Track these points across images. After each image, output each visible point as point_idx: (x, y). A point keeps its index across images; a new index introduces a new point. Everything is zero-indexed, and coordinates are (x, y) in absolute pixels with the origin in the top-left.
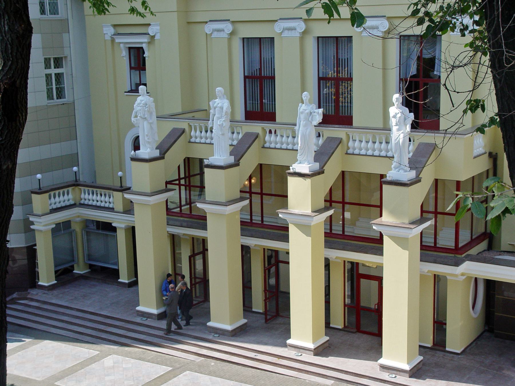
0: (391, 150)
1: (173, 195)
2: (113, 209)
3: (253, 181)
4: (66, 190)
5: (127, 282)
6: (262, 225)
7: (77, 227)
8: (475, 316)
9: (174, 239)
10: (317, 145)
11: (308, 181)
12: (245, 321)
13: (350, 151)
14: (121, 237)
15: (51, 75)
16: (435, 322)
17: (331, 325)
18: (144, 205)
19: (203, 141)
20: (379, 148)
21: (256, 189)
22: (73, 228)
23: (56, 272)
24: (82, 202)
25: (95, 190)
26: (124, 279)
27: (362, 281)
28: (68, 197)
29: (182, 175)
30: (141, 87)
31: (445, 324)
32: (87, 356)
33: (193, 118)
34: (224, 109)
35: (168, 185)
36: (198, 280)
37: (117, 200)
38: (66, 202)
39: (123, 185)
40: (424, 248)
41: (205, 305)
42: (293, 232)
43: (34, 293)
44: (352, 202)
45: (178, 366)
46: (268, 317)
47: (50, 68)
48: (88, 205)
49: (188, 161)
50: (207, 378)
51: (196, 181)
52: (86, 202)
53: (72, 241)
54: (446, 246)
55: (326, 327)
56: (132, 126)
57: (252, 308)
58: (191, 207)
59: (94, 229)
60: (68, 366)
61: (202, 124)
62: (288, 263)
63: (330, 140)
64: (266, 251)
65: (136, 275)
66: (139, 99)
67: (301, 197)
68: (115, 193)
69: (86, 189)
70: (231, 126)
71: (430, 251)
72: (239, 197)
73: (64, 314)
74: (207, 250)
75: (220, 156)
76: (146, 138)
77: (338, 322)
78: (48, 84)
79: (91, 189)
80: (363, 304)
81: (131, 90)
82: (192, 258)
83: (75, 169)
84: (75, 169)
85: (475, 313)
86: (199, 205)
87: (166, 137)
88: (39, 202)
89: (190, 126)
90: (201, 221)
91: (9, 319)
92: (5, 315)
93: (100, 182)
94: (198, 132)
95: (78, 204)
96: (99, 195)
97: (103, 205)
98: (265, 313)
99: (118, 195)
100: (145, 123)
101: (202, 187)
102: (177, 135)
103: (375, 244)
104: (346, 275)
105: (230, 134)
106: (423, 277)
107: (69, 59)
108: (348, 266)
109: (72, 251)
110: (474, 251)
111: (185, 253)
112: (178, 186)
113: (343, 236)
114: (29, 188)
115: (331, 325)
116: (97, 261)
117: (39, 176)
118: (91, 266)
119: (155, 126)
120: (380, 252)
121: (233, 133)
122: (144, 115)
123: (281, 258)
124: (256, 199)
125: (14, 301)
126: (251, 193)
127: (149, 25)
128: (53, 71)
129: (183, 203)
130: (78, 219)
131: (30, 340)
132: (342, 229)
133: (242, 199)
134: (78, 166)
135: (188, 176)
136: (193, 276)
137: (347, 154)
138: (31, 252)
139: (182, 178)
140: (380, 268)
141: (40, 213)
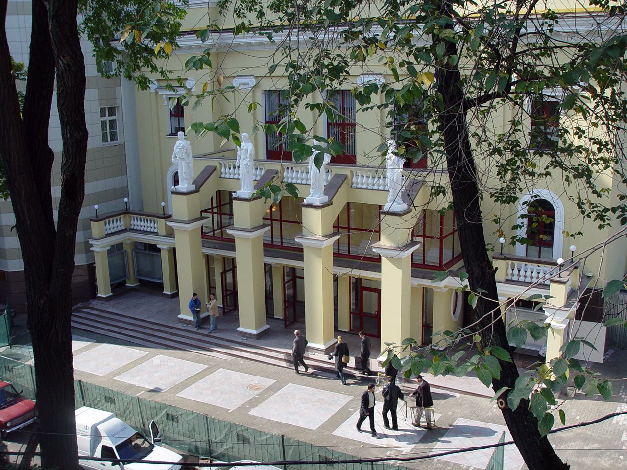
0: (310, 179)
1: (207, 222)
2: (157, 233)
3: (273, 209)
4: (118, 218)
5: (170, 293)
6: (281, 247)
7: (128, 248)
8: (455, 320)
9: (208, 258)
10: (327, 181)
11: (319, 211)
12: (268, 326)
13: (354, 185)
14: (165, 257)
15: (105, 122)
16: (423, 326)
17: (339, 329)
18: (182, 230)
19: (231, 176)
20: (379, 183)
21: (276, 216)
22: (124, 249)
23: (112, 286)
24: (132, 227)
25: (142, 217)
26: (167, 291)
27: (365, 292)
28: (119, 224)
29: (214, 205)
30: (180, 133)
31: (432, 327)
32: (139, 356)
33: (223, 158)
34: (249, 151)
35: (203, 213)
36: (228, 292)
37: (160, 226)
38: (119, 227)
39: (166, 213)
40: (414, 266)
41: (235, 312)
42: (385, 263)
43: (94, 303)
44: (355, 227)
45: (214, 364)
46: (287, 323)
47: (105, 116)
48: (137, 230)
49: (219, 193)
50: (237, 373)
51: (226, 209)
52: (135, 227)
53: (124, 259)
54: (433, 263)
55: (334, 330)
56: (172, 164)
57: (273, 315)
58: (222, 231)
59: (141, 250)
60: (123, 365)
61: (231, 162)
62: (303, 278)
63: (337, 176)
64: (285, 268)
65: (178, 289)
66: (178, 142)
67: (316, 224)
68: (158, 219)
69: (135, 216)
70: (255, 165)
71: (419, 268)
72: (262, 224)
73: (131, 324)
74: (236, 267)
75: (245, 190)
76: (184, 175)
77: (345, 326)
78: (103, 130)
79: (139, 217)
80: (365, 310)
81: (172, 133)
82: (224, 275)
83: (126, 200)
84: (126, 200)
85: (455, 318)
86: (229, 231)
87: (201, 173)
88: (96, 228)
89: (352, 173)
90: (230, 243)
91: (72, 324)
92: (69, 320)
93: (147, 210)
94: (227, 169)
95: (128, 229)
96: (146, 221)
97: (149, 229)
98: (285, 319)
99: (161, 221)
100: (183, 163)
101: (231, 215)
102: (210, 171)
103: (374, 262)
104: (352, 286)
105: (254, 171)
106: (414, 289)
107: (120, 108)
108: (353, 280)
109: (124, 266)
110: (454, 268)
111: (218, 270)
112: (211, 214)
113: (349, 256)
114: (89, 216)
115: (339, 329)
116: (145, 276)
117: (96, 206)
118: (140, 280)
119: (191, 165)
120: (378, 269)
121: (257, 169)
122: (182, 156)
123: (298, 274)
124: (276, 225)
125: (78, 310)
126: (272, 220)
127: (187, 79)
128: (107, 118)
129: (216, 227)
130: (129, 242)
131: (89, 343)
132: (422, 259)
133: (264, 226)
134: (128, 197)
135: (220, 206)
136: (225, 289)
137: (351, 188)
138: (91, 269)
139: (215, 207)
140: (379, 282)
141: (98, 237)
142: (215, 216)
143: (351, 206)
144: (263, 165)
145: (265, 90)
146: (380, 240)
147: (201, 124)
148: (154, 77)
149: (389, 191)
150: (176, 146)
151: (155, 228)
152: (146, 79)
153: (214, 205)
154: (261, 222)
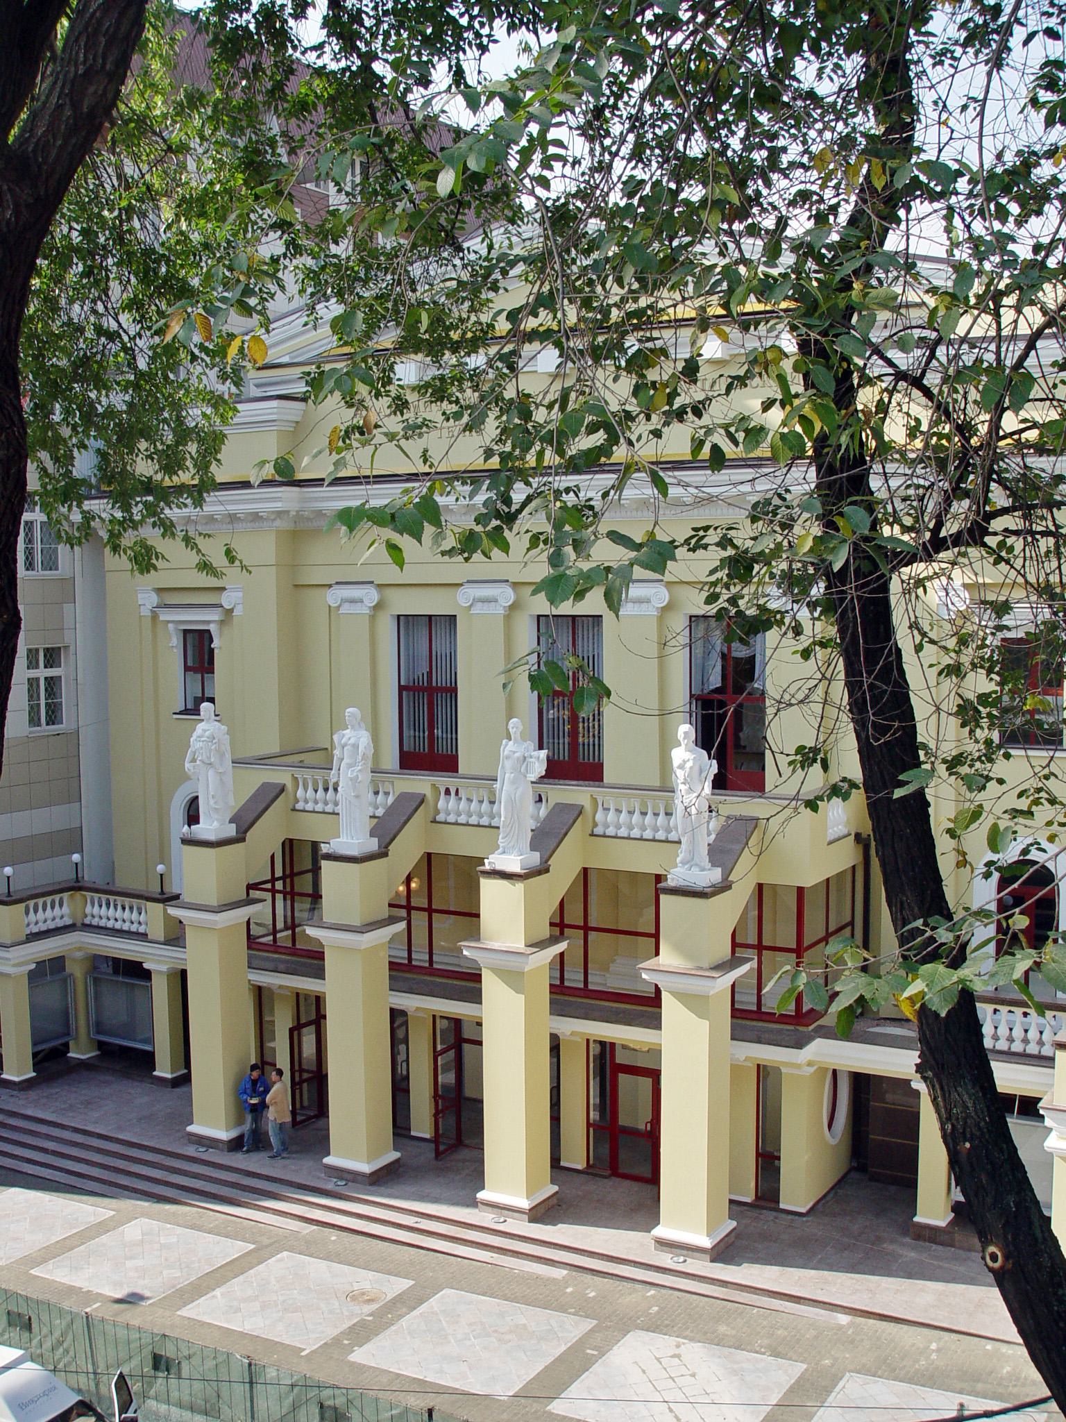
1: (261, 911)
3: (413, 885)
10: (536, 818)
11: (520, 886)
19: (319, 807)
20: (652, 825)
29: (279, 873)
30: (205, 706)
33: (301, 765)
39: (166, 889)
49: (289, 846)
56: (185, 777)
61: (319, 775)
63: (561, 808)
66: (201, 726)
70: (373, 781)
75: (352, 837)
76: (212, 802)
89: (594, 801)
100: (211, 773)
101: (316, 896)
102: (270, 795)
105: (371, 795)
121: (376, 793)
122: (209, 758)
124: (420, 919)
126: (409, 908)
129: (280, 925)
133: (392, 920)
135: (290, 875)
137: (592, 835)
139: (279, 879)
142: (279, 897)
143: (592, 878)
145: (399, 616)
146: (657, 954)
149: (679, 842)
150: (195, 735)
151: (140, 923)
153: (279, 873)
154: (385, 912)
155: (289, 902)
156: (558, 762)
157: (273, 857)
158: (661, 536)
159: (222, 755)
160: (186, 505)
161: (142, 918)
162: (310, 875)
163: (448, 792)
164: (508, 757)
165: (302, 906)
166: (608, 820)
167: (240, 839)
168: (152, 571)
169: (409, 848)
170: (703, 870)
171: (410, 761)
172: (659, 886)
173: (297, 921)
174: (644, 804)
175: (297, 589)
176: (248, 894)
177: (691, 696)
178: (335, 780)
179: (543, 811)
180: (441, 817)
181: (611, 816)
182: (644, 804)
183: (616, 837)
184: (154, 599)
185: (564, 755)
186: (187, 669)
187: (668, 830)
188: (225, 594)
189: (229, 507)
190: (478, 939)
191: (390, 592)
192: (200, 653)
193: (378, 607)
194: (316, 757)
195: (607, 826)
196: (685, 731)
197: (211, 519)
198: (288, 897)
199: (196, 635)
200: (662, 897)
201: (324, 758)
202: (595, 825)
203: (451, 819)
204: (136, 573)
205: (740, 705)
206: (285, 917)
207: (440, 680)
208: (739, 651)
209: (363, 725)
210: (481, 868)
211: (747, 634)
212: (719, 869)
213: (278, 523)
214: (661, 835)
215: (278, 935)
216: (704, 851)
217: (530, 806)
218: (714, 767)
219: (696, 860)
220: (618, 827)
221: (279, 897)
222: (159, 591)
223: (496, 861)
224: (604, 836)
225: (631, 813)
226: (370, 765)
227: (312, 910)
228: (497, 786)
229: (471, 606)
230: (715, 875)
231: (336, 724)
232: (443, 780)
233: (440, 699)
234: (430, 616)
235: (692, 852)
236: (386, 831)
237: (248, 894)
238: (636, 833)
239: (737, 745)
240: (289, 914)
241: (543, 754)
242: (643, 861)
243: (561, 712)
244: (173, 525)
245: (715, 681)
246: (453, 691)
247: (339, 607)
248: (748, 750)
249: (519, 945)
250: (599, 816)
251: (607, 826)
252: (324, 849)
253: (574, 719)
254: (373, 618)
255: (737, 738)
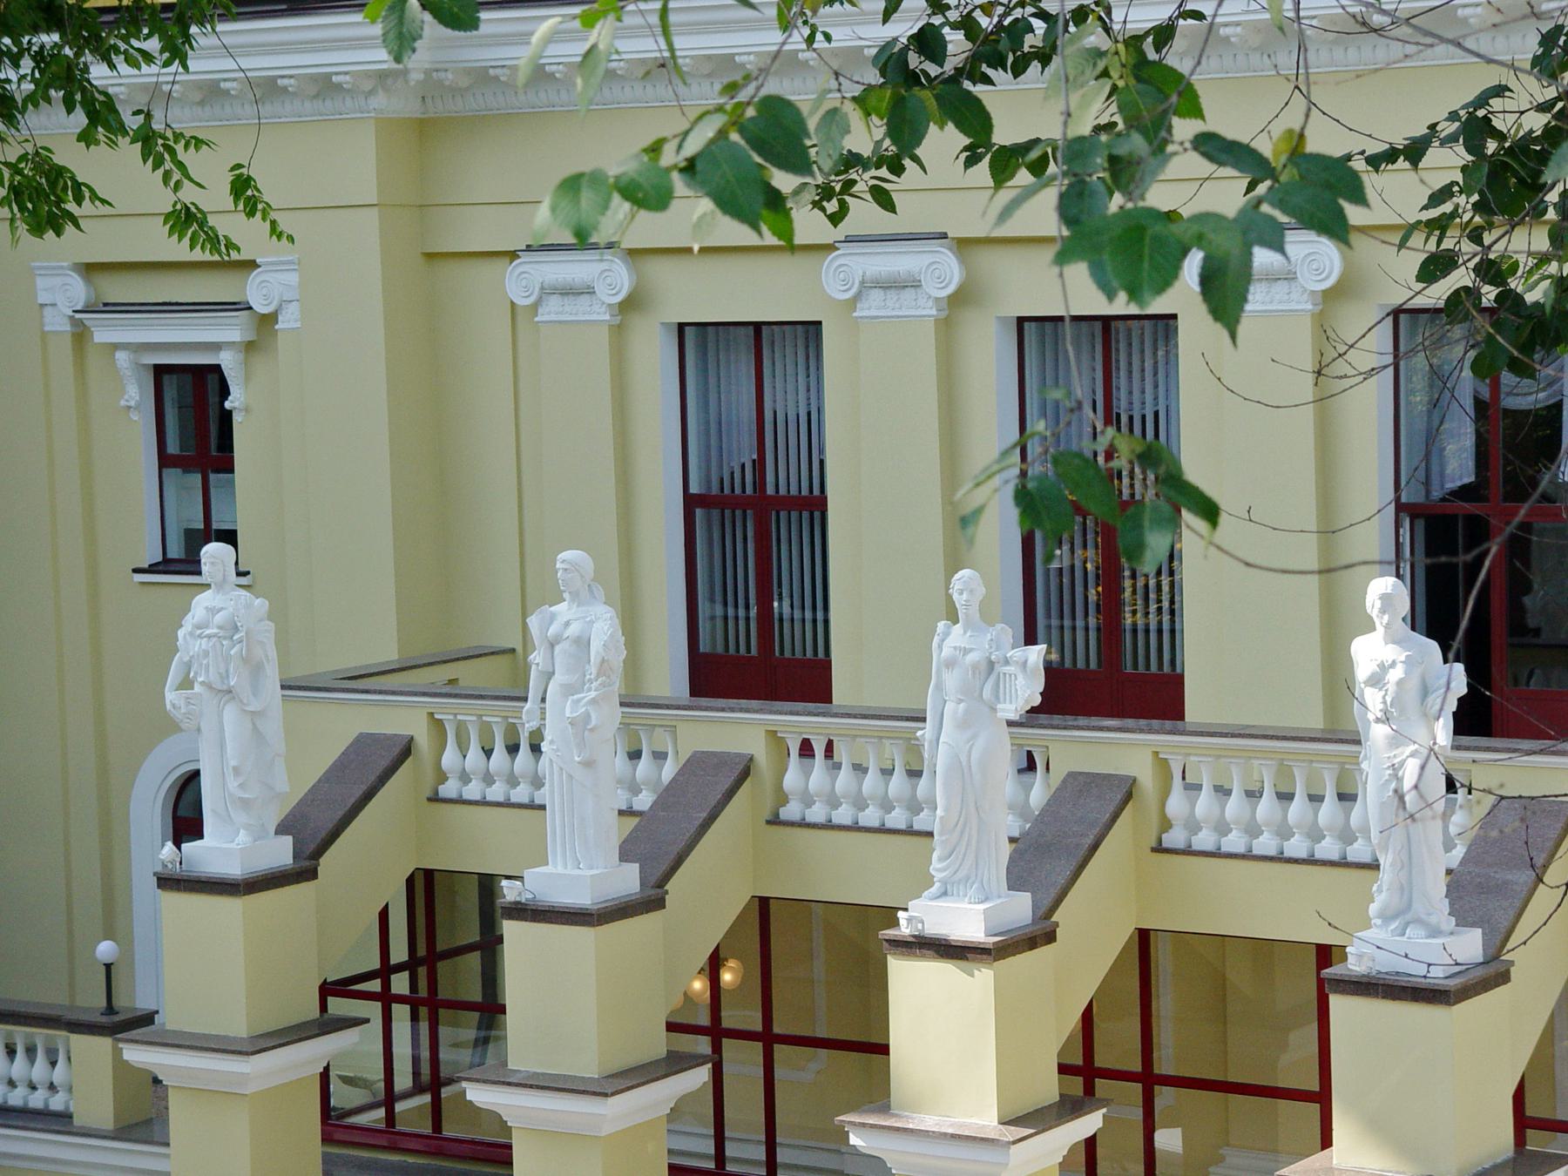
1: (354, 1049)
3: (727, 977)
10: (1022, 810)
11: (984, 977)
19: (496, 792)
20: (1308, 825)
29: (399, 953)
30: (213, 552)
33: (452, 690)
34: (596, 646)
39: (120, 1001)
49: (425, 887)
51: (463, 978)
56: (170, 726)
61: (495, 715)
63: (1081, 785)
66: (203, 601)
70: (625, 726)
75: (574, 861)
76: (232, 784)
89: (1162, 766)
94: (474, 755)
99: (92, 1050)
100: (230, 713)
101: (491, 1009)
102: (376, 766)
105: (621, 761)
119: (273, 728)
121: (635, 755)
122: (225, 677)
124: (743, 1060)
126: (716, 1032)
129: (403, 1081)
133: (675, 1063)
135: (428, 957)
137: (1159, 849)
139: (399, 968)
142: (401, 1012)
143: (1162, 956)
144: (673, 730)
145: (681, 327)
146: (1326, 1142)
147: (596, 178)
148: (111, 169)
149: (1374, 866)
150: (189, 622)
151: (52, 1087)
152: (57, 174)
153: (399, 953)
154: (658, 1043)
155: (424, 1027)
156: (1074, 673)
157: (384, 915)
158: (1324, 141)
159: (256, 670)
160: (148, 57)
161: (59, 1074)
162: (474, 960)
163: (806, 749)
164: (950, 664)
165: (458, 1033)
166: (1195, 813)
167: (303, 871)
168: (69, 228)
169: (711, 894)
170: (1435, 932)
171: (714, 677)
172: (1327, 972)
173: (444, 1072)
174: (1284, 772)
175: (432, 263)
176: (324, 1007)
177: (1400, 507)
178: (534, 724)
179: (1039, 792)
180: (791, 811)
181: (1205, 803)
182: (1284, 772)
183: (1216, 854)
184: (77, 291)
185: (1087, 656)
186: (165, 461)
187: (1347, 837)
188: (255, 278)
189: (245, 63)
190: (885, 1109)
191: (660, 270)
192: (196, 421)
193: (631, 305)
194: (476, 666)
195: (1194, 827)
196: (1384, 593)
197: (212, 92)
198: (423, 1011)
199: (189, 378)
200: (1337, 1002)
201: (502, 672)
202: (1166, 825)
203: (817, 814)
204: (22, 228)
205: (1526, 527)
206: (416, 1060)
207: (784, 479)
208: (1522, 396)
209: (600, 592)
210: (890, 933)
211: (1527, 347)
212: (1477, 933)
213: (379, 101)
214: (1328, 848)
215: (400, 1107)
216: (1436, 886)
217: (1006, 782)
218: (1458, 679)
219: (1418, 908)
220: (1223, 829)
221: (401, 1012)
222: (90, 270)
223: (926, 914)
224: (1188, 852)
225: (1253, 795)
226: (617, 686)
227: (482, 1042)
228: (926, 733)
229: (857, 297)
230: (1470, 946)
231: (536, 590)
232: (795, 722)
233: (786, 527)
234: (758, 327)
235: (1406, 889)
236: (661, 845)
237: (324, 1007)
238: (1266, 844)
239: (1519, 626)
240: (425, 1054)
241: (1036, 654)
242: (1287, 913)
243: (1079, 552)
244: (110, 104)
245: (1458, 463)
246: (815, 505)
247: (535, 307)
248: (1544, 638)
249: (984, 1118)
250: (1176, 804)
251: (1194, 827)
252: (510, 892)
253: (1110, 575)
254: (618, 332)
255: (1517, 611)
